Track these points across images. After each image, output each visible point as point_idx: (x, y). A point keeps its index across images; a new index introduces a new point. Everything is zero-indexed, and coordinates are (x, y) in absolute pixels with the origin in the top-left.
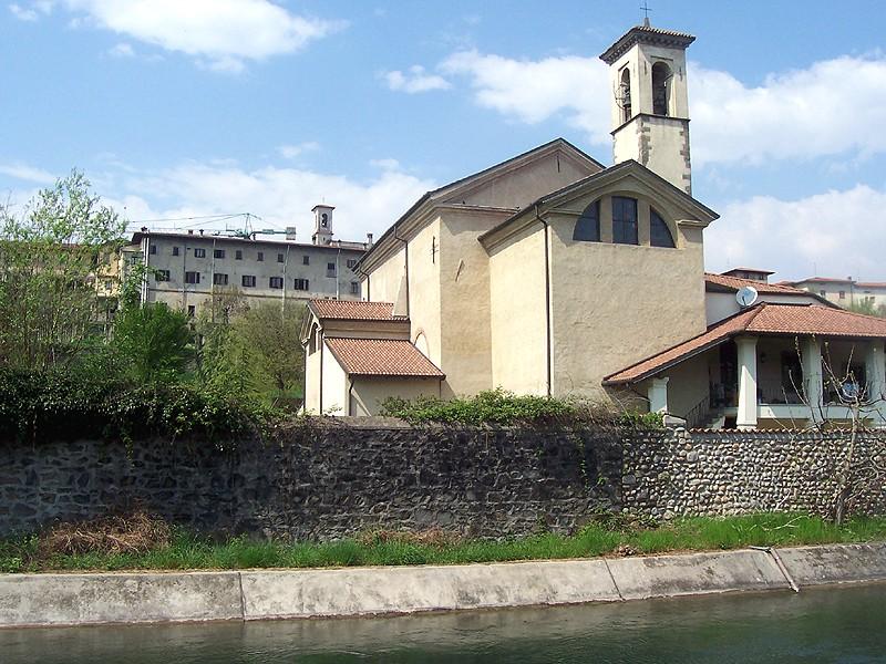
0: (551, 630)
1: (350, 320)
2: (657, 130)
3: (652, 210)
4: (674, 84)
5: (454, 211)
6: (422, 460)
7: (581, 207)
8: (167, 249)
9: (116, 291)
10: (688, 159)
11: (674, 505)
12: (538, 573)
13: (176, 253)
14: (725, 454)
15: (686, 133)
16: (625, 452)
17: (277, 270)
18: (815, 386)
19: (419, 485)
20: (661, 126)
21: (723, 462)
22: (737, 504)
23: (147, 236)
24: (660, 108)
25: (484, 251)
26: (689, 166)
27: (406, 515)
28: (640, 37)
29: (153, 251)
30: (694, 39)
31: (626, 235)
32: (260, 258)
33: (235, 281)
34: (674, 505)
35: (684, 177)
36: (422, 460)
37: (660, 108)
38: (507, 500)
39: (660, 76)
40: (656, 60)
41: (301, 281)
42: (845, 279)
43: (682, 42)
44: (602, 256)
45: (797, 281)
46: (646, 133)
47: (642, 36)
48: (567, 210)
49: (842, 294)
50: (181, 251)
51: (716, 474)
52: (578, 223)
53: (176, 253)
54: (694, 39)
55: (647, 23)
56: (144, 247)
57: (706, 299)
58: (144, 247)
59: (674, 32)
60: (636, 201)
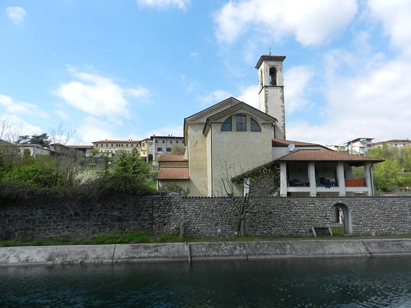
0: (29, 273)
1: (179, 161)
2: (271, 91)
3: (251, 118)
4: (278, 74)
5: (193, 124)
6: (75, 208)
7: (223, 120)
8: (161, 141)
9: (146, 155)
10: (283, 100)
11: (174, 224)
12: (85, 249)
13: (164, 142)
14: (197, 205)
15: (282, 91)
16: (154, 205)
17: (169, 146)
18: (342, 181)
19: (74, 217)
20: (272, 90)
21: (196, 209)
22: (202, 225)
23: (154, 137)
24: (274, 83)
25: (204, 136)
26: (283, 103)
27: (67, 227)
28: (265, 59)
29: (156, 142)
30: (285, 57)
31: (241, 128)
32: (171, 142)
33: (164, 149)
34: (174, 224)
35: (282, 107)
36: (75, 208)
37: (274, 83)
38: (107, 222)
39: (273, 72)
40: (271, 66)
41: (169, 148)
42: (405, 139)
43: (281, 59)
44: (232, 136)
45: (385, 141)
46: (267, 93)
47: (264, 58)
48: (219, 121)
49: (396, 145)
50: (165, 141)
51: (193, 213)
52: (223, 125)
53: (164, 142)
54: (285, 57)
55: (270, 54)
56: (154, 141)
57: (272, 150)
58: (154, 141)
59: (276, 55)
60: (245, 116)
